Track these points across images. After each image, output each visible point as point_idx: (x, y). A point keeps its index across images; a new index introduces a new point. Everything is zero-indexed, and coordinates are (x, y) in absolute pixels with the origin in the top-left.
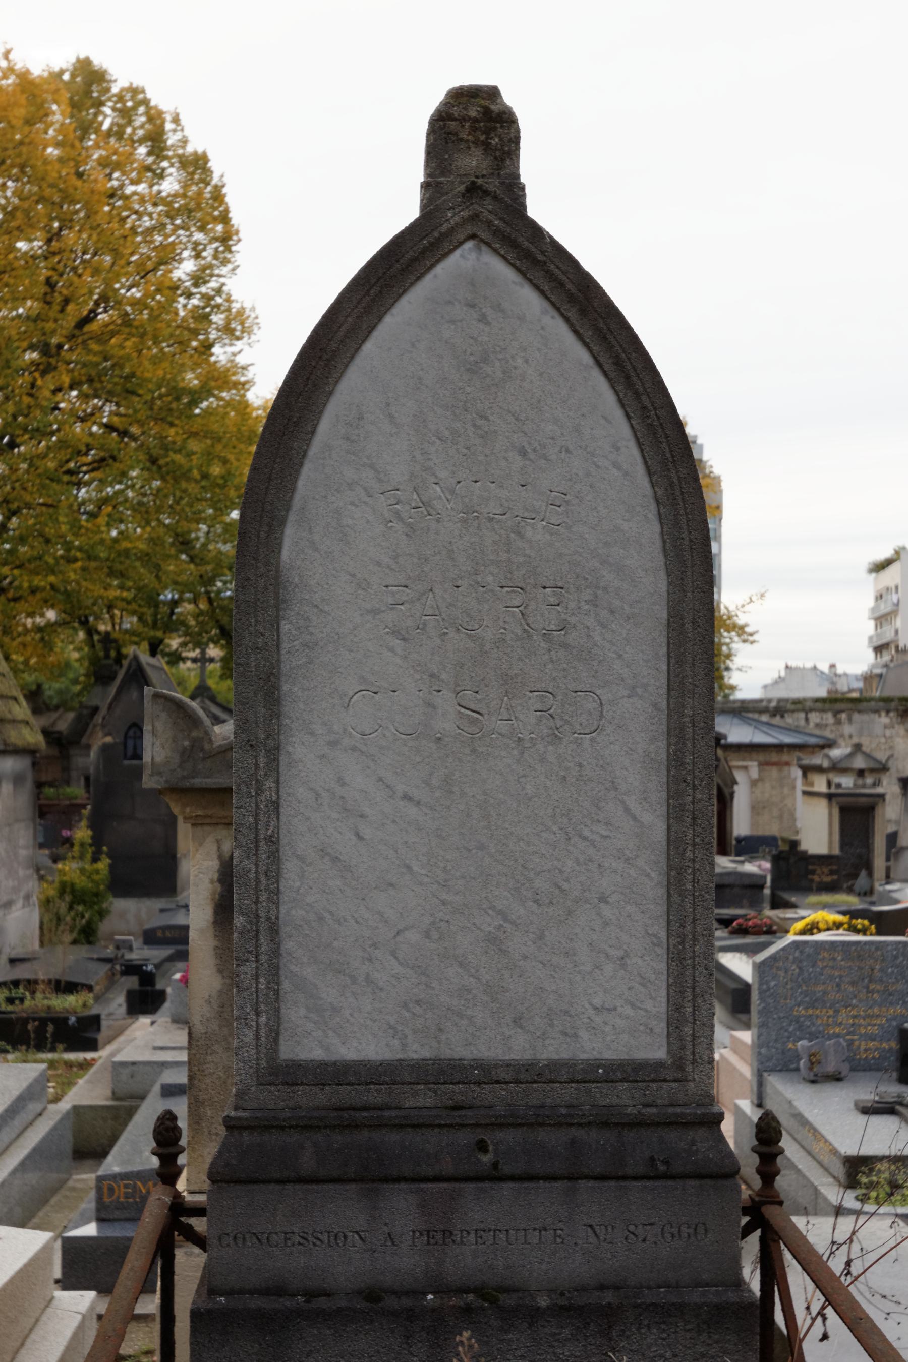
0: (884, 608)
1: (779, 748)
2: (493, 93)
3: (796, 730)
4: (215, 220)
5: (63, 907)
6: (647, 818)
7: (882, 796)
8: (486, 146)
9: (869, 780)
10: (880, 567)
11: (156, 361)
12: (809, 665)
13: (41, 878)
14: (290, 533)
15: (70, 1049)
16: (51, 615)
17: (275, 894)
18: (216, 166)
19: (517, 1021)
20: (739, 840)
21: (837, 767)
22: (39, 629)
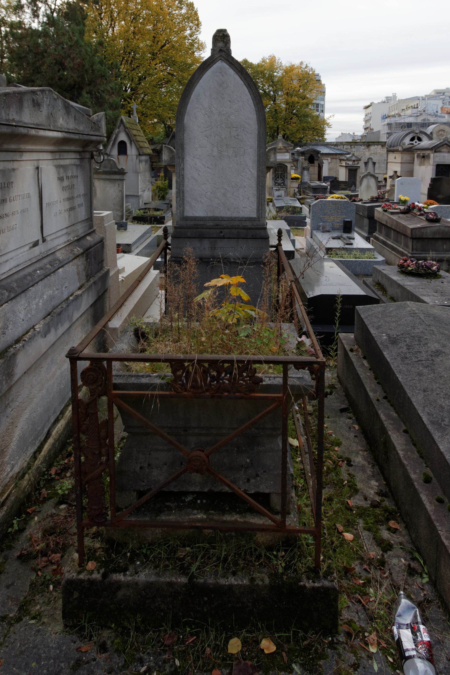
0: (367, 118)
1: (336, 154)
2: (225, 31)
3: (341, 150)
4: (195, 20)
5: (157, 191)
6: (253, 172)
7: (359, 167)
8: (223, 41)
9: (356, 163)
10: (367, 107)
11: (180, 56)
12: (348, 133)
13: (152, 185)
14: (186, 117)
15: (157, 224)
16: (156, 120)
17: (183, 186)
18: (196, 6)
19: (228, 210)
20: (324, 177)
21: (348, 160)
22: (153, 124)
